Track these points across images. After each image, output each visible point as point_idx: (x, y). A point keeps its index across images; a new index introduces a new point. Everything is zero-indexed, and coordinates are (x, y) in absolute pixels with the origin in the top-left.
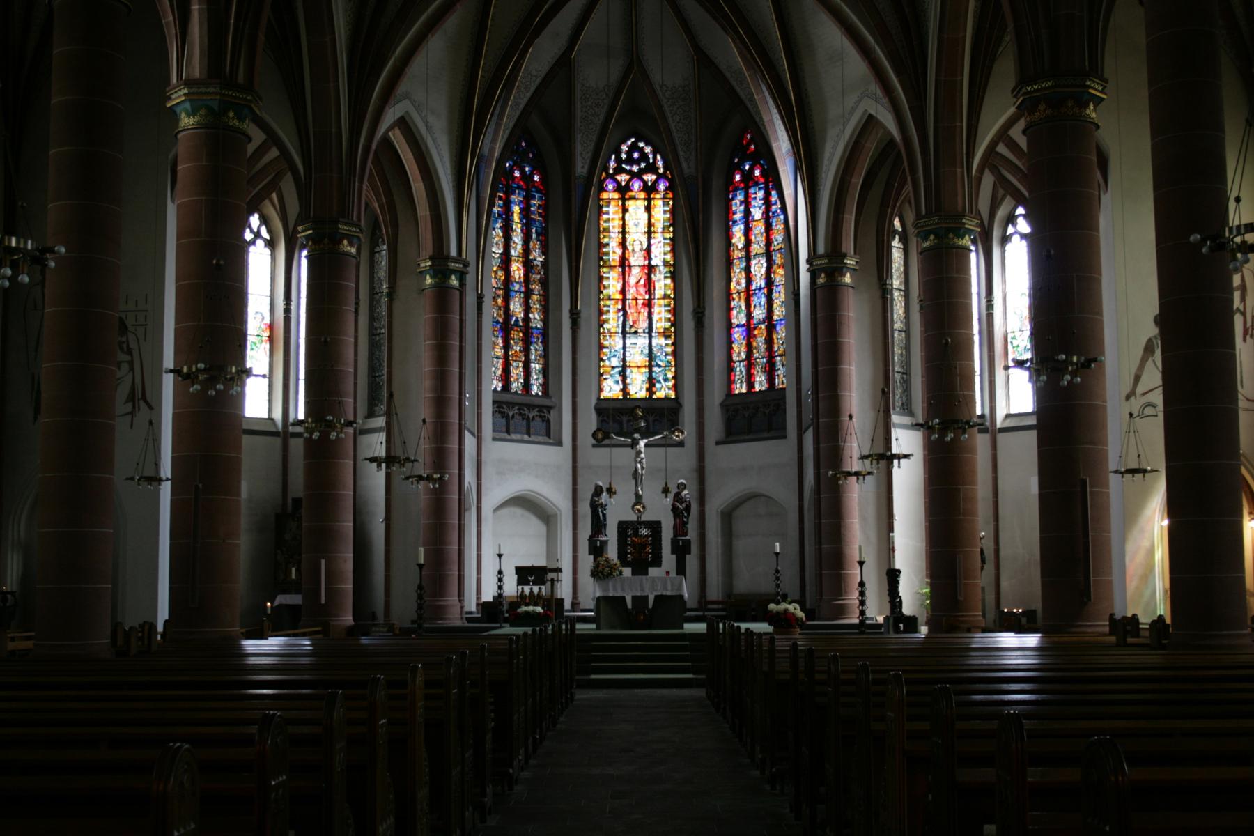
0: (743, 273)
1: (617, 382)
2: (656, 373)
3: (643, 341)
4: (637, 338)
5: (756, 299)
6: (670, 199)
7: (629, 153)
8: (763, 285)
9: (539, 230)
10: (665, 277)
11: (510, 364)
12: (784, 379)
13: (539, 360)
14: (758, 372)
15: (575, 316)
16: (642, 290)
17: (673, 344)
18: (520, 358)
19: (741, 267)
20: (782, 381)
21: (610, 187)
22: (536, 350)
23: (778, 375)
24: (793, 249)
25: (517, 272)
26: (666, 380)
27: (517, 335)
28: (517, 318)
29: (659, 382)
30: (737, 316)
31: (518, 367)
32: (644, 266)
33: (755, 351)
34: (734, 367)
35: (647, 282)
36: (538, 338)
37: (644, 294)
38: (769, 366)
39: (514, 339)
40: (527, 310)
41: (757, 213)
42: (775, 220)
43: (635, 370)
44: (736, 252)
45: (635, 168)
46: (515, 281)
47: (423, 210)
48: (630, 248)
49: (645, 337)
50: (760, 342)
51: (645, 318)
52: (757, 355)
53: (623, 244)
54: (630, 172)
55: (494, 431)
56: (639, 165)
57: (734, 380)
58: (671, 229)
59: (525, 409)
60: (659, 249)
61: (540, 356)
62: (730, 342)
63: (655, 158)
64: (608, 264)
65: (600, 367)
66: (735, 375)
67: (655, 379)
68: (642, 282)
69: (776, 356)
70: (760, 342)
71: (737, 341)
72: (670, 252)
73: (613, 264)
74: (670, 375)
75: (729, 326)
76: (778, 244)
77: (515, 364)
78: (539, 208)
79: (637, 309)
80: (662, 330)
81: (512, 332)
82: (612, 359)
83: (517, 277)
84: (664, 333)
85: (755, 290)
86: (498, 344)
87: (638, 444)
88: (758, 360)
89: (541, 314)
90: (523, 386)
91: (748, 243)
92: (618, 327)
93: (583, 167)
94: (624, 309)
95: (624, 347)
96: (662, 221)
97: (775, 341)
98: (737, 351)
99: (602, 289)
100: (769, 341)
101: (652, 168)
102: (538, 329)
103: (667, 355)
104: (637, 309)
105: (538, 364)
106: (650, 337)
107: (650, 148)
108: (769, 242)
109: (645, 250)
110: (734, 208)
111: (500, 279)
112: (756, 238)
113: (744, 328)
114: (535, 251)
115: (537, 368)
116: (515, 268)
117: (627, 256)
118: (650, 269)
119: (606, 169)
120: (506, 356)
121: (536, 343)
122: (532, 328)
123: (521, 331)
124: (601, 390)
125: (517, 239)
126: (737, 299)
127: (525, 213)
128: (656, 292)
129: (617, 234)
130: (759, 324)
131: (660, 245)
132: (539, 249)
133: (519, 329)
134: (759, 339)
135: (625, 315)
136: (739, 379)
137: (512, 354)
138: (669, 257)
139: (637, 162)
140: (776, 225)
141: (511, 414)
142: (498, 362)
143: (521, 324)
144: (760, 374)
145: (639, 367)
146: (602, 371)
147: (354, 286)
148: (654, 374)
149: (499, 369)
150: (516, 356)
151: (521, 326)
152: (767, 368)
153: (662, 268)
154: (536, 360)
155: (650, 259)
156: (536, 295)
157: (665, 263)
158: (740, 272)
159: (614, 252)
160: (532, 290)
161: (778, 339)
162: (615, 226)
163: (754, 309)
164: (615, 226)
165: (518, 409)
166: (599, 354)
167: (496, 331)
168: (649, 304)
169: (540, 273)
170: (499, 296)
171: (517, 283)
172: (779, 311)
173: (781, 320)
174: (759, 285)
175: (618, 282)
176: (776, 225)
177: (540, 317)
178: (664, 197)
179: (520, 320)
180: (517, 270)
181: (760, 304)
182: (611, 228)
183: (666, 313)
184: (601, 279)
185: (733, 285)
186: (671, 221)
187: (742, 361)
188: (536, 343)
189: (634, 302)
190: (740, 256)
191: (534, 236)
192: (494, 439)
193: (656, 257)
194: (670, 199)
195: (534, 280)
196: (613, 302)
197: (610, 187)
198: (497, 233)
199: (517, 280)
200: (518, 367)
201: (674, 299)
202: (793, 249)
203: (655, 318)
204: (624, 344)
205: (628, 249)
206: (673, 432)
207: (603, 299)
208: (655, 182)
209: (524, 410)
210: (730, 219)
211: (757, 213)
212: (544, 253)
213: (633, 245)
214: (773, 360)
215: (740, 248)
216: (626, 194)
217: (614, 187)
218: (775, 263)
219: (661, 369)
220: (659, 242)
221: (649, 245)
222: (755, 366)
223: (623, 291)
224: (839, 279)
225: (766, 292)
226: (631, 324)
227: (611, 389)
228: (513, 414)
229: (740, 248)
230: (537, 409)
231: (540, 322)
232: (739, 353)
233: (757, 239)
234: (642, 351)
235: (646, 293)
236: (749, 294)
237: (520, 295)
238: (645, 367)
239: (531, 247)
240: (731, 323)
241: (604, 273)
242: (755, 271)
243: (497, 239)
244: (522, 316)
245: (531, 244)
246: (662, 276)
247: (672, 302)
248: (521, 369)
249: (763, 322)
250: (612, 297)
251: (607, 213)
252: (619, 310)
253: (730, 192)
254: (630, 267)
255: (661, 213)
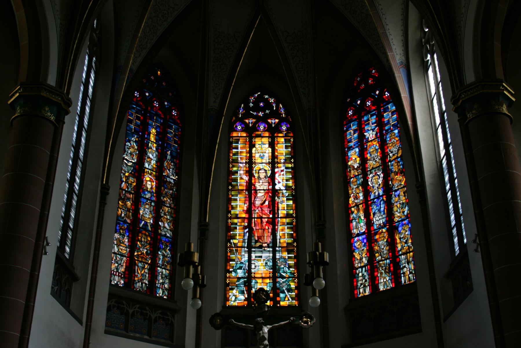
0: (360, 188)
1: (242, 292)
2: (280, 284)
3: (267, 255)
4: (262, 251)
5: (375, 207)
6: (291, 137)
7: (256, 103)
8: (381, 193)
9: (174, 154)
10: (287, 200)
11: (135, 264)
12: (410, 275)
13: (166, 266)
14: (381, 273)
15: (203, 228)
16: (266, 211)
17: (295, 257)
18: (146, 259)
19: (358, 182)
20: (409, 277)
21: (239, 128)
22: (164, 255)
23: (404, 273)
24: (414, 145)
25: (149, 183)
26: (289, 290)
27: (144, 239)
28: (146, 223)
29: (283, 292)
30: (356, 226)
31: (143, 268)
32: (268, 190)
33: (377, 255)
34: (356, 273)
35: (271, 203)
36: (167, 247)
37: (268, 213)
38: (394, 267)
39: (141, 241)
40: (157, 218)
41: (370, 135)
42: (388, 136)
43: (260, 281)
44: (352, 172)
45: (261, 114)
46: (147, 190)
47: (24, 41)
48: (256, 175)
49: (269, 251)
50: (382, 244)
51: (270, 234)
52: (380, 257)
53: (250, 172)
54: (257, 117)
55: (106, 326)
56: (264, 111)
57: (357, 285)
58: (292, 160)
59: (147, 308)
60: (282, 176)
61: (168, 263)
62: (351, 250)
63: (278, 107)
64: (236, 188)
65: (226, 278)
66: (357, 282)
67: (279, 289)
68: (267, 203)
69: (401, 255)
70: (382, 244)
71: (358, 248)
72: (292, 178)
73: (240, 188)
74: (293, 286)
75: (350, 236)
76: (394, 155)
77: (140, 265)
78: (175, 136)
79: (262, 226)
80: (285, 245)
81: (140, 235)
82: (238, 271)
83: (149, 187)
84: (286, 247)
85: (374, 199)
86: (123, 243)
87: (261, 329)
88: (381, 262)
89: (171, 224)
90: (147, 287)
91: (364, 161)
92: (244, 241)
93: (215, 102)
94: (249, 226)
95: (250, 260)
96: (284, 154)
97: (398, 241)
98: (358, 258)
99: (230, 209)
100: (392, 243)
101: (275, 114)
102: (167, 237)
103: (289, 267)
104: (262, 226)
105: (165, 269)
106: (274, 252)
107: (272, 217)
108: (384, 156)
109: (269, 177)
110: (348, 137)
111: (131, 184)
112: (371, 155)
113: (364, 236)
114: (169, 170)
115: (164, 273)
116: (148, 179)
117: (253, 181)
118: (274, 193)
119: (236, 113)
120: (131, 256)
121: (165, 249)
122: (161, 235)
123: (149, 236)
124: (227, 299)
125: (152, 155)
126: (356, 212)
127: (161, 137)
128: (280, 212)
129: (244, 164)
130: (380, 229)
131: (282, 173)
132: (173, 169)
133: (147, 233)
134: (380, 243)
135: (251, 232)
136: (361, 284)
137: (138, 255)
138: (290, 183)
139: (263, 109)
140: (390, 140)
141: (131, 311)
142: (121, 260)
143: (150, 228)
144: (384, 275)
145: (263, 278)
146: (228, 281)
147: (34, 241)
148: (278, 285)
149: (122, 266)
150: (142, 258)
151: (149, 231)
152: (392, 268)
153: (284, 191)
154: (163, 265)
155: (274, 185)
156: (167, 207)
157: (287, 188)
158: (358, 187)
159: (241, 178)
160: (164, 202)
161: (400, 239)
162: (242, 158)
163: (373, 217)
164: (242, 158)
165: (139, 308)
166: (226, 266)
167: (123, 230)
168: (273, 222)
169: (172, 190)
170: (129, 199)
171: (149, 192)
172: (400, 212)
173: (402, 220)
174: (377, 194)
175: (245, 204)
176: (390, 140)
177: (170, 227)
178: (286, 135)
179: (149, 225)
180: (149, 182)
181: (379, 210)
182: (239, 159)
183: (288, 230)
184: (229, 201)
185: (351, 200)
186: (292, 154)
187: (364, 266)
188: (165, 249)
189: (259, 220)
190: (357, 174)
191: (169, 157)
192: (106, 332)
193: (279, 182)
194: (291, 137)
195: (166, 194)
196: (240, 220)
197: (239, 128)
198: (132, 146)
199: (149, 190)
200: (143, 268)
201: (296, 218)
202: (414, 145)
203: (279, 234)
204: (250, 257)
205: (254, 177)
206: (301, 319)
207: (231, 218)
208: (279, 125)
209: (146, 310)
210: (346, 146)
211: (370, 135)
212: (177, 173)
213: (259, 173)
214: (398, 259)
215: (356, 167)
216: (253, 133)
217: (242, 128)
218: (392, 172)
219: (285, 280)
220: (282, 171)
221: (273, 173)
222: (378, 268)
223: (249, 211)
224: (497, 107)
225: (385, 199)
226: (257, 239)
227: (236, 298)
228: (133, 312)
229: (356, 167)
230: (160, 311)
231: (169, 231)
232: (361, 259)
233: (373, 155)
234: (266, 263)
235: (270, 213)
236: (367, 204)
237: (151, 203)
238: (269, 278)
239: (165, 165)
240: (352, 234)
241: (232, 196)
242: (372, 183)
243: (131, 150)
244: (152, 222)
245: (166, 164)
246: (285, 199)
247: (294, 221)
248: (146, 271)
249: (384, 225)
250: (239, 216)
251: (237, 148)
252: (245, 228)
253: (344, 125)
254: (256, 191)
255: (282, 150)
